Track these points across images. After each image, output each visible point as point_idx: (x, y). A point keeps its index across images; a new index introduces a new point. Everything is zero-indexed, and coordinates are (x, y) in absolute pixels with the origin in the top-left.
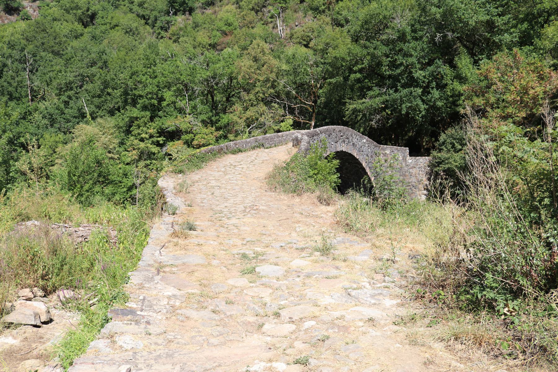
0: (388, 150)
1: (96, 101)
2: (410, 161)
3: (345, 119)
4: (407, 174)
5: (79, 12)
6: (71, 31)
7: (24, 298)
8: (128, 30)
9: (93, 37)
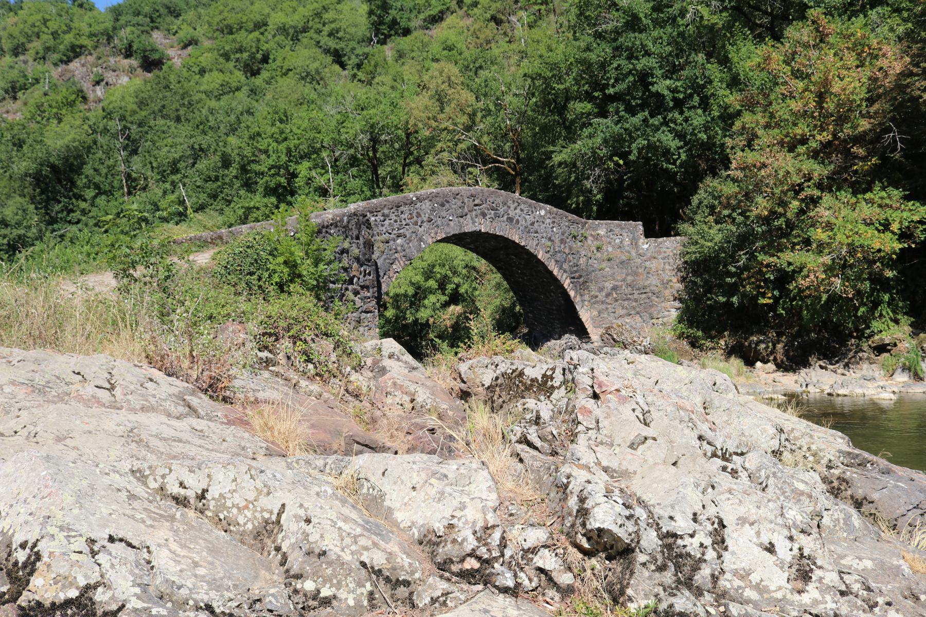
1: (210, 186)
2: (646, 246)
3: (557, 182)
4: (640, 270)
5: (245, 55)
6: (222, 85)
8: (304, 74)
9: (252, 90)
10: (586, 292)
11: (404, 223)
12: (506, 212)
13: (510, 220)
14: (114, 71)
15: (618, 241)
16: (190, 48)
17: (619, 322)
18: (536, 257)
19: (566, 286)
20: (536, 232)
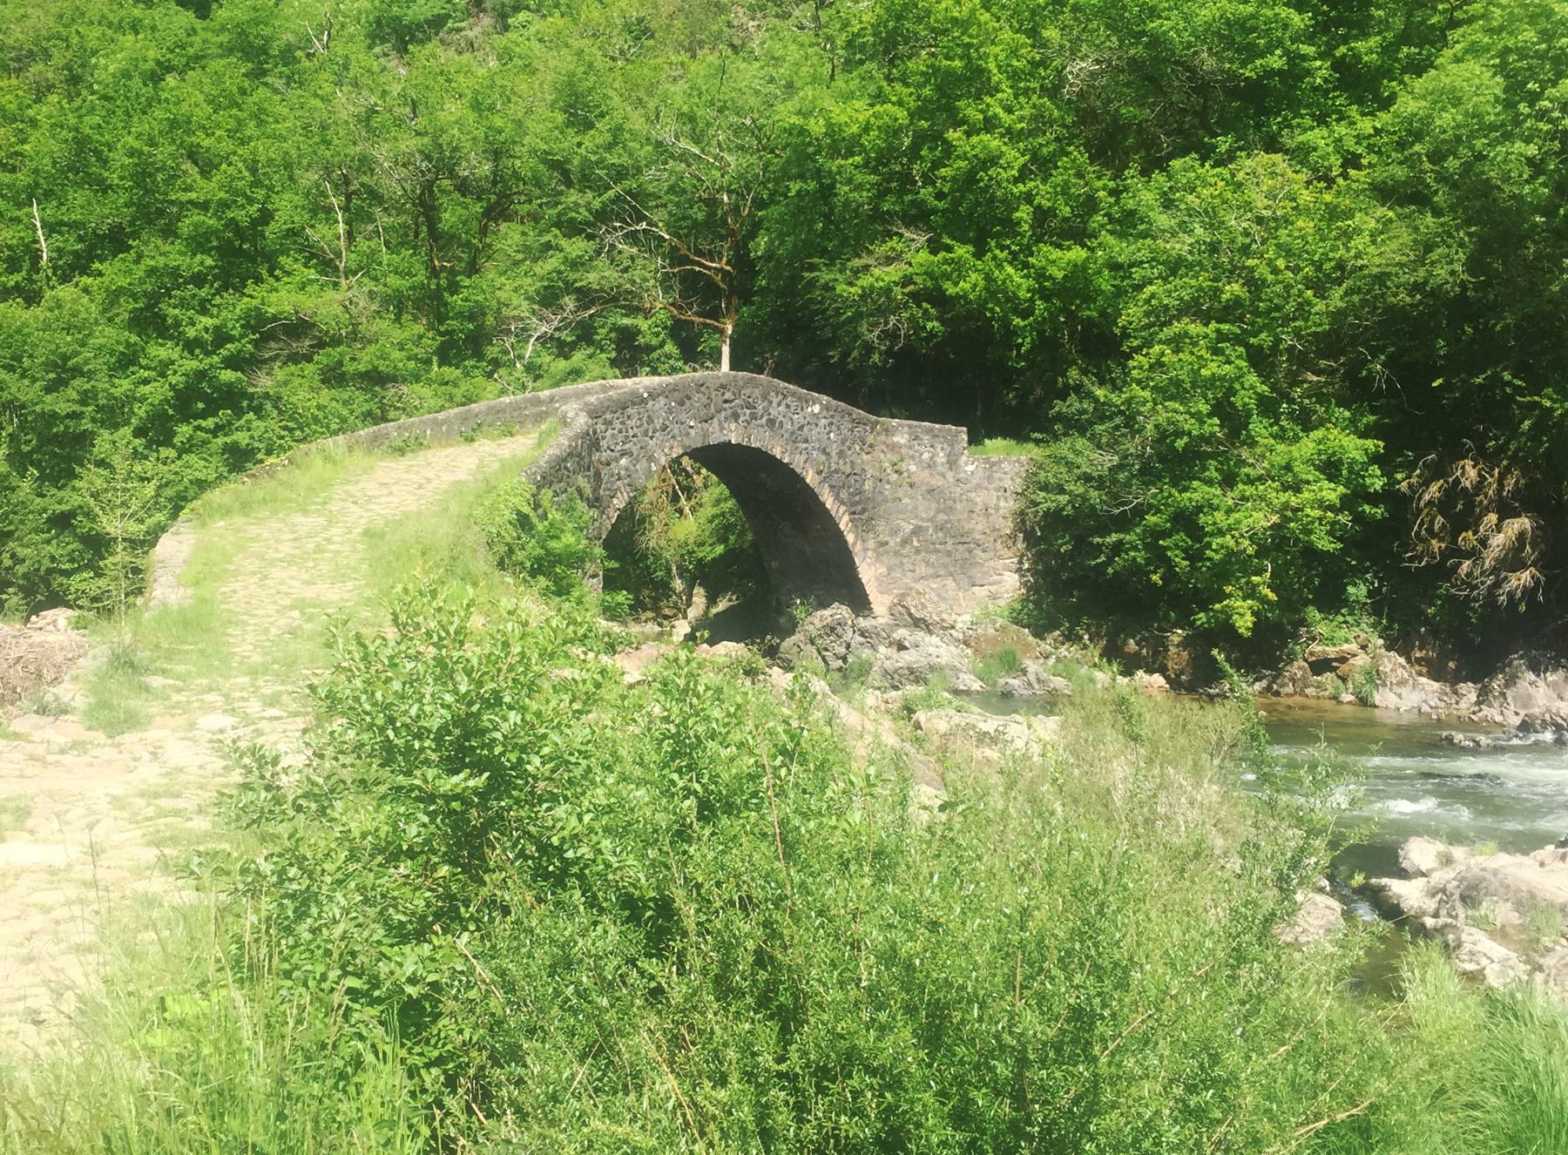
0: (902, 431)
2: (970, 468)
7: (579, 201)
12: (766, 410)
15: (926, 456)
17: (920, 587)
19: (842, 527)
20: (806, 441)
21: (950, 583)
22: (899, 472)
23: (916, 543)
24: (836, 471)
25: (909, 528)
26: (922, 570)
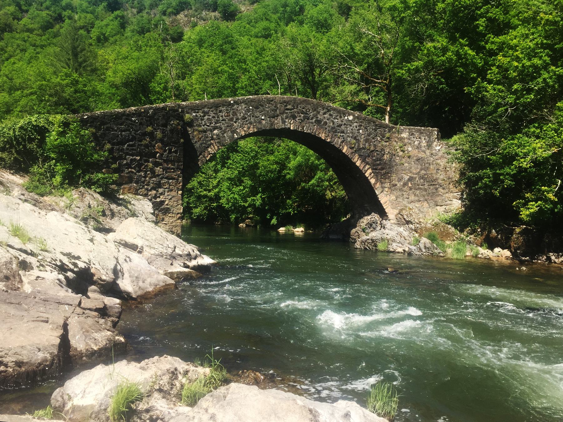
2: (438, 148)
10: (387, 181)
11: (221, 119)
12: (315, 116)
13: (318, 122)
14: (204, 20)
15: (416, 143)
16: (255, 4)
17: (411, 206)
18: (341, 151)
19: (367, 175)
20: (343, 132)
21: (426, 204)
22: (403, 151)
23: (410, 185)
24: (364, 148)
25: (406, 178)
26: (412, 198)
